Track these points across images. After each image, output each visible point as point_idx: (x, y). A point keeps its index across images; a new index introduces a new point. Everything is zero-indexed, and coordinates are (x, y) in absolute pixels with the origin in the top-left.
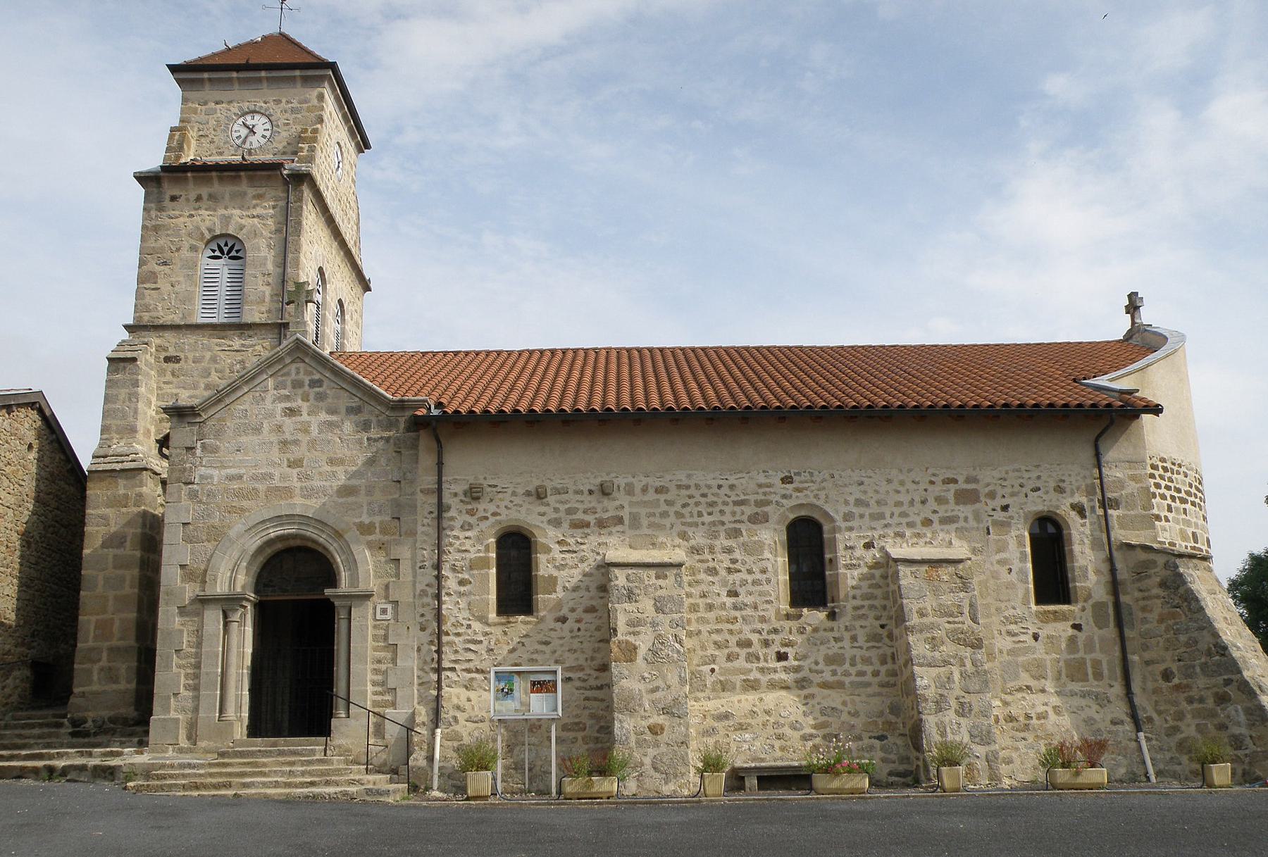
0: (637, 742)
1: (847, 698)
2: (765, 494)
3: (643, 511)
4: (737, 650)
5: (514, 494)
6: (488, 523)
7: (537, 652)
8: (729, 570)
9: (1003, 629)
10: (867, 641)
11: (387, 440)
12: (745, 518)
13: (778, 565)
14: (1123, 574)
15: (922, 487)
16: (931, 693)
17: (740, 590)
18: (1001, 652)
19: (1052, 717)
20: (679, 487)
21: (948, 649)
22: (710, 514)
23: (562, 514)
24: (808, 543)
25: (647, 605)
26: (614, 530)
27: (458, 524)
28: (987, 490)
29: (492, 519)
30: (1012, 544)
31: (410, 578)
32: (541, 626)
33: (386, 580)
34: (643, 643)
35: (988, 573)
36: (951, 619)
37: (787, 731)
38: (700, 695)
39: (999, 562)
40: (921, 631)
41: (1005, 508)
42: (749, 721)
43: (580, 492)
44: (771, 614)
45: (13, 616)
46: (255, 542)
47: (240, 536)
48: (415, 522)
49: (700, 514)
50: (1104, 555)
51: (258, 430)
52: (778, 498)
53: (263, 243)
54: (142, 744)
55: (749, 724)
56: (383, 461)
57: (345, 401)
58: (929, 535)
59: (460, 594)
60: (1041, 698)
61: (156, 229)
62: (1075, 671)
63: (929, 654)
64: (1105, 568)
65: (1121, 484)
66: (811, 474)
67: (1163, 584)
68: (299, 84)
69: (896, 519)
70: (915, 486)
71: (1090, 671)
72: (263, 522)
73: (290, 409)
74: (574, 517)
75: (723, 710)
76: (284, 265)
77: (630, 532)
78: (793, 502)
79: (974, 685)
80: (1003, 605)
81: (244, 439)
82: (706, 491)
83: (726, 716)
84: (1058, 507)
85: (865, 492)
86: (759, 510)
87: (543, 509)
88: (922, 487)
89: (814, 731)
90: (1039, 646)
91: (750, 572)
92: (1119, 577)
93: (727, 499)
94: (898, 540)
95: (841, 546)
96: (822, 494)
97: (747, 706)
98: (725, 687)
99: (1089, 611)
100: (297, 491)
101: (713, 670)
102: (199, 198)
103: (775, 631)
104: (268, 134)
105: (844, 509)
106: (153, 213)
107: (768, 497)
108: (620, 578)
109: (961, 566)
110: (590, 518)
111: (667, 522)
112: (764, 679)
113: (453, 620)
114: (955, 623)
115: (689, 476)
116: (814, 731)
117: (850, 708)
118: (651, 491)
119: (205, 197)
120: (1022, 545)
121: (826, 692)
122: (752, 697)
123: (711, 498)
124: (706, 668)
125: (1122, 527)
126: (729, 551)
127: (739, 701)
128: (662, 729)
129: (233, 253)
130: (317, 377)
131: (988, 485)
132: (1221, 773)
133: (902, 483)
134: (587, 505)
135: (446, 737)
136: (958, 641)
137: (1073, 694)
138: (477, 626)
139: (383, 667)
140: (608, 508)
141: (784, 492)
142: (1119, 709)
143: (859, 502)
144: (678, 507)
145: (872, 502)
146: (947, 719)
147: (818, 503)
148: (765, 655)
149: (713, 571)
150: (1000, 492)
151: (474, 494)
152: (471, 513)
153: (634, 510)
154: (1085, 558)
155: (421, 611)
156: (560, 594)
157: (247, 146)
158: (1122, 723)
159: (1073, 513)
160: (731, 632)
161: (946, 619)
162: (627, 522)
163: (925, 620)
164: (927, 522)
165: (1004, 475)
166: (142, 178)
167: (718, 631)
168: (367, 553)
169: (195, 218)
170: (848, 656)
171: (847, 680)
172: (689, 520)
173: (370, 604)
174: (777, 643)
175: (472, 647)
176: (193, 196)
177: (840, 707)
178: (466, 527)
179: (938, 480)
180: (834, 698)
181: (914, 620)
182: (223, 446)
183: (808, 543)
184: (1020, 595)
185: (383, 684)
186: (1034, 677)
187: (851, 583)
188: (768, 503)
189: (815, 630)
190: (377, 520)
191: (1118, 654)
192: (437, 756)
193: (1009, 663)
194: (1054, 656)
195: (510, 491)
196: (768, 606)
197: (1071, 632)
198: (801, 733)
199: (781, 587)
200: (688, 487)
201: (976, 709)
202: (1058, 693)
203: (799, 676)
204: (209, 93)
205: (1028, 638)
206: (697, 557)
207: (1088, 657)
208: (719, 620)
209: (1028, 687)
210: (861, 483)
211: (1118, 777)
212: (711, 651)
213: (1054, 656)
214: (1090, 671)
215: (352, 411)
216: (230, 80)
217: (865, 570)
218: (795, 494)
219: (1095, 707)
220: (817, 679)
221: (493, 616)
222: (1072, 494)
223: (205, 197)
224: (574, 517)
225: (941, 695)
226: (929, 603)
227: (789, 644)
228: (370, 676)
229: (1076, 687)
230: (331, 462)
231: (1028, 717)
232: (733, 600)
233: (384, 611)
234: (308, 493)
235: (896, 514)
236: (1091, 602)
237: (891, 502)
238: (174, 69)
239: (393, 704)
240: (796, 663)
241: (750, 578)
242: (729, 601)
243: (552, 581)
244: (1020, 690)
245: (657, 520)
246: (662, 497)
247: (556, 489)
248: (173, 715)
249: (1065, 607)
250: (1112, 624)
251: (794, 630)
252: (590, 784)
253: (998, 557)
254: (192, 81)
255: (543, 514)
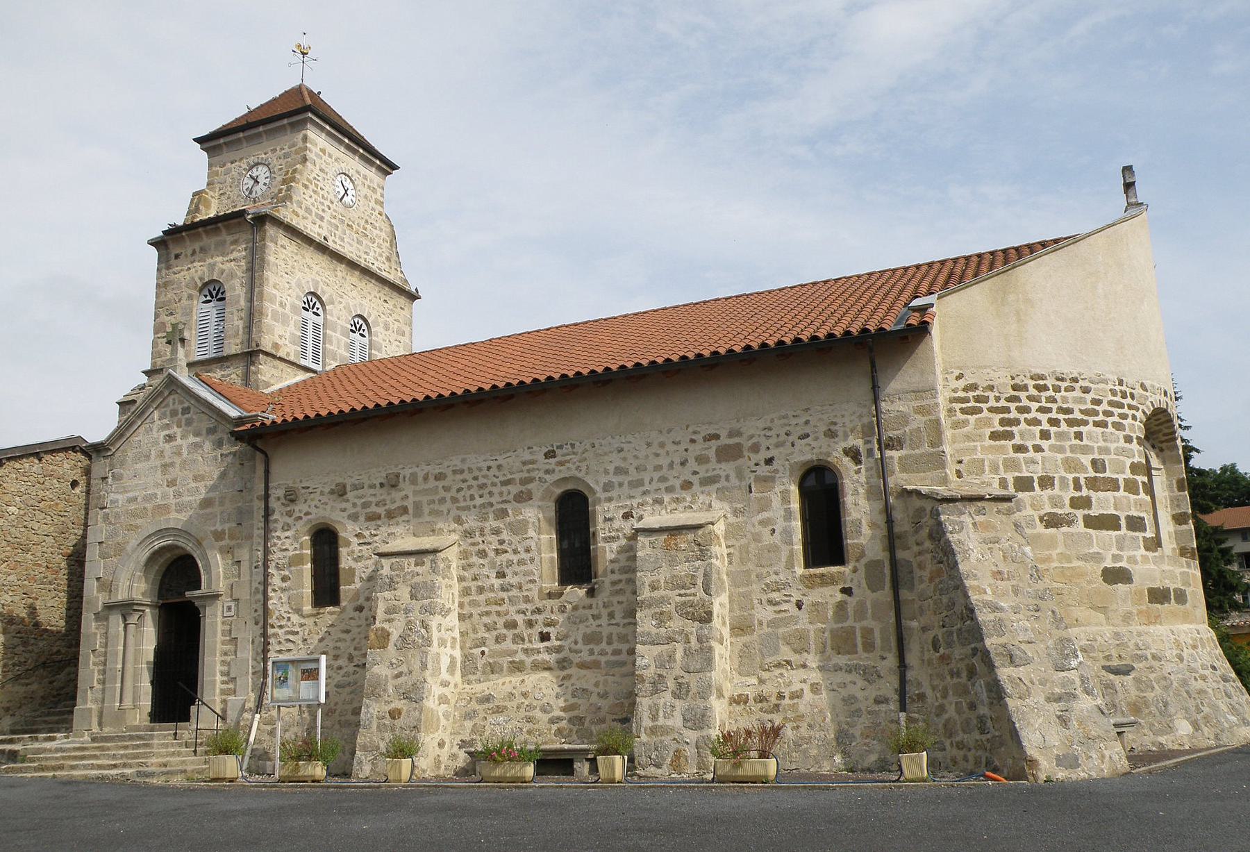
0: (378, 727)
1: (601, 679)
2: (528, 471)
3: (425, 499)
4: (504, 631)
5: (322, 493)
6: (301, 522)
7: (339, 640)
8: (497, 552)
9: (764, 598)
10: (624, 618)
11: (234, 454)
12: (511, 497)
13: (544, 545)
14: (903, 523)
15: (682, 447)
16: (649, 673)
17: (506, 571)
18: (761, 623)
19: (808, 695)
20: (454, 472)
21: (676, 624)
22: (481, 496)
23: (359, 509)
24: (573, 516)
25: (404, 592)
26: (400, 519)
27: (279, 526)
28: (750, 443)
29: (305, 518)
30: (776, 501)
31: (248, 578)
32: (343, 616)
33: (232, 580)
34: (395, 631)
35: (749, 536)
36: (683, 592)
37: (538, 713)
38: (472, 677)
39: (762, 523)
40: (650, 606)
41: (769, 461)
42: (506, 703)
43: (372, 486)
44: (535, 594)
45: (62, 623)
46: (145, 554)
47: (134, 550)
48: (252, 526)
49: (472, 498)
50: (879, 505)
51: (147, 457)
52: (541, 474)
53: (237, 282)
54: (69, 729)
55: (506, 708)
56: (231, 474)
57: (206, 424)
58: (688, 499)
59: (283, 590)
60: (802, 674)
61: (166, 285)
62: (842, 642)
63: (654, 631)
64: (881, 520)
65: (904, 419)
66: (573, 446)
67: (931, 536)
68: (245, 144)
69: (655, 485)
70: (675, 447)
71: (859, 641)
72: (149, 536)
73: (169, 436)
74: (368, 510)
75: (487, 693)
76: (251, 300)
77: (414, 521)
78: (556, 477)
79: (695, 664)
80: (764, 571)
81: (138, 466)
82: (476, 473)
83: (488, 699)
84: (829, 454)
85: (625, 459)
86: (523, 488)
87: (344, 505)
88: (682, 447)
89: (562, 714)
90: (803, 615)
91: (515, 552)
92: (897, 530)
93: (495, 480)
94: (657, 507)
95: (600, 519)
96: (583, 466)
97: (508, 688)
98: (493, 669)
99: (862, 571)
100: (173, 507)
101: (483, 653)
102: (194, 253)
103: (538, 611)
104: (267, 181)
105: (604, 479)
106: (164, 271)
107: (532, 474)
108: (644, 548)
109: (700, 532)
110: (381, 510)
111: (444, 508)
112: (528, 660)
113: (277, 614)
114: (686, 595)
115: (463, 461)
116: (562, 714)
117: (601, 689)
118: (431, 478)
119: (198, 250)
120: (786, 499)
121: (583, 672)
122: (515, 679)
123: (482, 481)
124: (477, 651)
125: (904, 469)
126: (497, 532)
127: (504, 684)
128: (400, 713)
129: (220, 296)
130: (186, 405)
131: (752, 437)
132: (916, 765)
133: (662, 445)
134: (379, 498)
135: (262, 721)
136: (686, 616)
137: (837, 669)
138: (295, 618)
139: (228, 659)
140: (395, 499)
141: (547, 467)
142: (889, 686)
143: (619, 471)
144: (453, 493)
145: (632, 470)
146: (662, 702)
147: (580, 475)
148: (530, 636)
149: (482, 554)
150: (764, 443)
151: (291, 497)
152: (289, 514)
153: (417, 499)
154: (858, 509)
155: (255, 606)
156: (358, 584)
157: (254, 195)
158: (886, 701)
159: (846, 460)
160: (498, 613)
161: (678, 592)
162: (411, 511)
163: (656, 594)
164: (687, 485)
165: (769, 424)
166: (155, 243)
167: (488, 613)
168: (218, 556)
169: (195, 271)
170: (605, 634)
171: (603, 659)
172: (462, 504)
173: (219, 603)
174: (540, 622)
175: (291, 637)
176: (189, 252)
177: (591, 688)
178: (287, 527)
179: (699, 438)
180: (588, 679)
181: (646, 594)
182: (126, 473)
183: (573, 516)
184: (784, 559)
185: (228, 674)
186: (795, 651)
187: (610, 556)
188: (531, 480)
189: (575, 608)
190: (227, 526)
191: (893, 620)
192: (252, 739)
193: (768, 635)
194: (820, 625)
195: (318, 491)
196: (531, 586)
197: (840, 597)
198: (550, 715)
199: (546, 566)
200: (462, 472)
201: (694, 689)
202: (821, 668)
203: (561, 656)
204: (227, 155)
205: (791, 607)
206: (470, 541)
207: (858, 625)
208: (488, 602)
209: (788, 662)
210: (621, 450)
211: (866, 765)
212: (482, 633)
213: (820, 625)
214: (859, 641)
215: (211, 431)
216: (239, 140)
217: (624, 542)
218: (558, 469)
219: (861, 683)
220: (576, 659)
221: (308, 608)
222: (846, 437)
223: (198, 250)
224: (368, 510)
225: (660, 676)
226: (663, 575)
227: (549, 624)
228: (219, 668)
229: (842, 660)
230: (196, 478)
231: (781, 696)
232: (500, 581)
233: (229, 608)
234: (181, 508)
235: (655, 479)
236: (864, 561)
237: (650, 467)
238: (195, 140)
239: (234, 692)
240: (558, 643)
241: (515, 558)
242: (497, 583)
243: (352, 571)
244: (779, 665)
245: (436, 507)
246: (440, 484)
247: (354, 485)
248: (89, 706)
249: (834, 569)
250: (888, 585)
251: (556, 610)
252: (297, 768)
253: (760, 517)
254: (214, 148)
255: (344, 510)
